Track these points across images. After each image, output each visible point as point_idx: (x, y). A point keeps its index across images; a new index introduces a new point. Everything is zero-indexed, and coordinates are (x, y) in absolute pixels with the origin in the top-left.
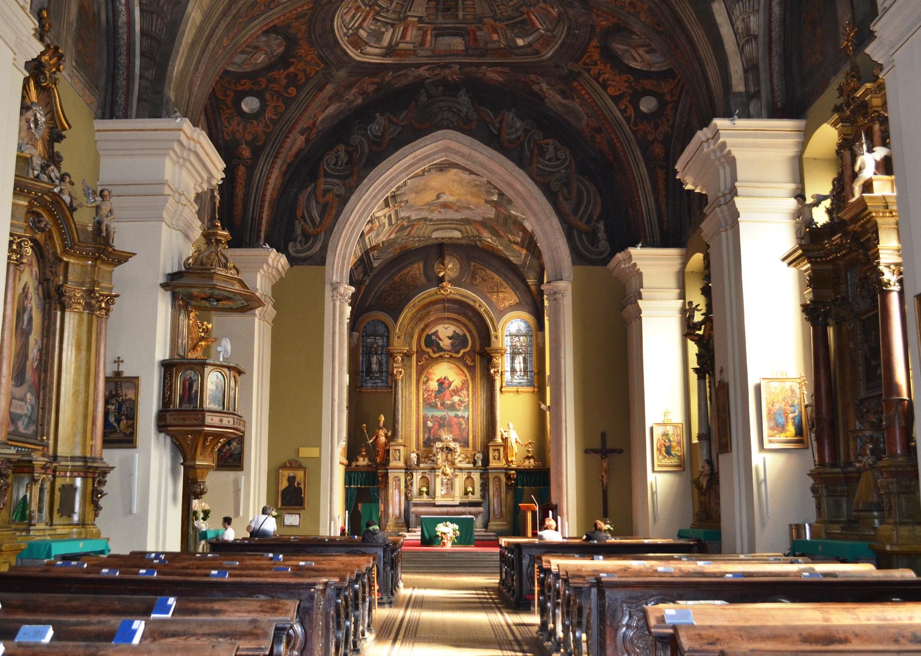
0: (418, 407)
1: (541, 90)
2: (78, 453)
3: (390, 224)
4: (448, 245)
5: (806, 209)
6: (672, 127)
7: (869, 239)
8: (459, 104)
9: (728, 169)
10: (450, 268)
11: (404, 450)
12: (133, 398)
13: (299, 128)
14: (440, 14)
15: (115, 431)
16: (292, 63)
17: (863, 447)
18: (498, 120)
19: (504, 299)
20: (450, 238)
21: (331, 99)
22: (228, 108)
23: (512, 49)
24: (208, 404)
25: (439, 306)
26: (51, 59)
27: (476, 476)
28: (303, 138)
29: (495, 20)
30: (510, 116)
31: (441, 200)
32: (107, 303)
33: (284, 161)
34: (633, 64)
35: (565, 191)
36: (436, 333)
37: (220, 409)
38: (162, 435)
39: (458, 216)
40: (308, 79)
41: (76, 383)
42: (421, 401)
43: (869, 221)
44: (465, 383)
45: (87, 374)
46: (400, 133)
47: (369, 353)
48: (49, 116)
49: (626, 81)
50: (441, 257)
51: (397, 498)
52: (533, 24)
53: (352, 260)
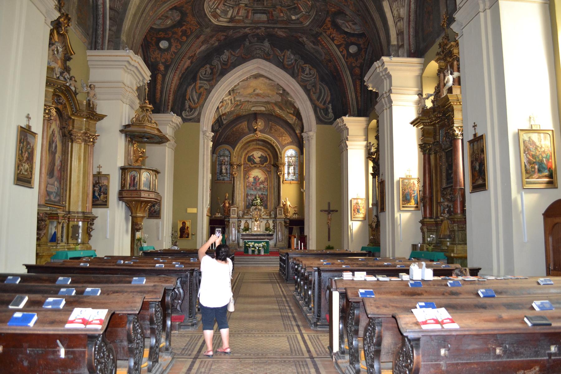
1: (303, 41)
2: (80, 210)
3: (231, 103)
9: (388, 80)
10: (260, 124)
13: (187, 56)
15: (98, 200)
16: (184, 25)
17: (444, 210)
18: (283, 54)
19: (285, 140)
20: (260, 111)
21: (203, 43)
23: (290, 21)
25: (255, 143)
27: (271, 222)
28: (189, 61)
32: (93, 139)
33: (180, 72)
34: (346, 30)
35: (314, 89)
36: (253, 155)
37: (148, 189)
38: (121, 202)
39: (264, 100)
40: (192, 33)
43: (450, 106)
44: (266, 179)
47: (221, 164)
52: (300, 9)
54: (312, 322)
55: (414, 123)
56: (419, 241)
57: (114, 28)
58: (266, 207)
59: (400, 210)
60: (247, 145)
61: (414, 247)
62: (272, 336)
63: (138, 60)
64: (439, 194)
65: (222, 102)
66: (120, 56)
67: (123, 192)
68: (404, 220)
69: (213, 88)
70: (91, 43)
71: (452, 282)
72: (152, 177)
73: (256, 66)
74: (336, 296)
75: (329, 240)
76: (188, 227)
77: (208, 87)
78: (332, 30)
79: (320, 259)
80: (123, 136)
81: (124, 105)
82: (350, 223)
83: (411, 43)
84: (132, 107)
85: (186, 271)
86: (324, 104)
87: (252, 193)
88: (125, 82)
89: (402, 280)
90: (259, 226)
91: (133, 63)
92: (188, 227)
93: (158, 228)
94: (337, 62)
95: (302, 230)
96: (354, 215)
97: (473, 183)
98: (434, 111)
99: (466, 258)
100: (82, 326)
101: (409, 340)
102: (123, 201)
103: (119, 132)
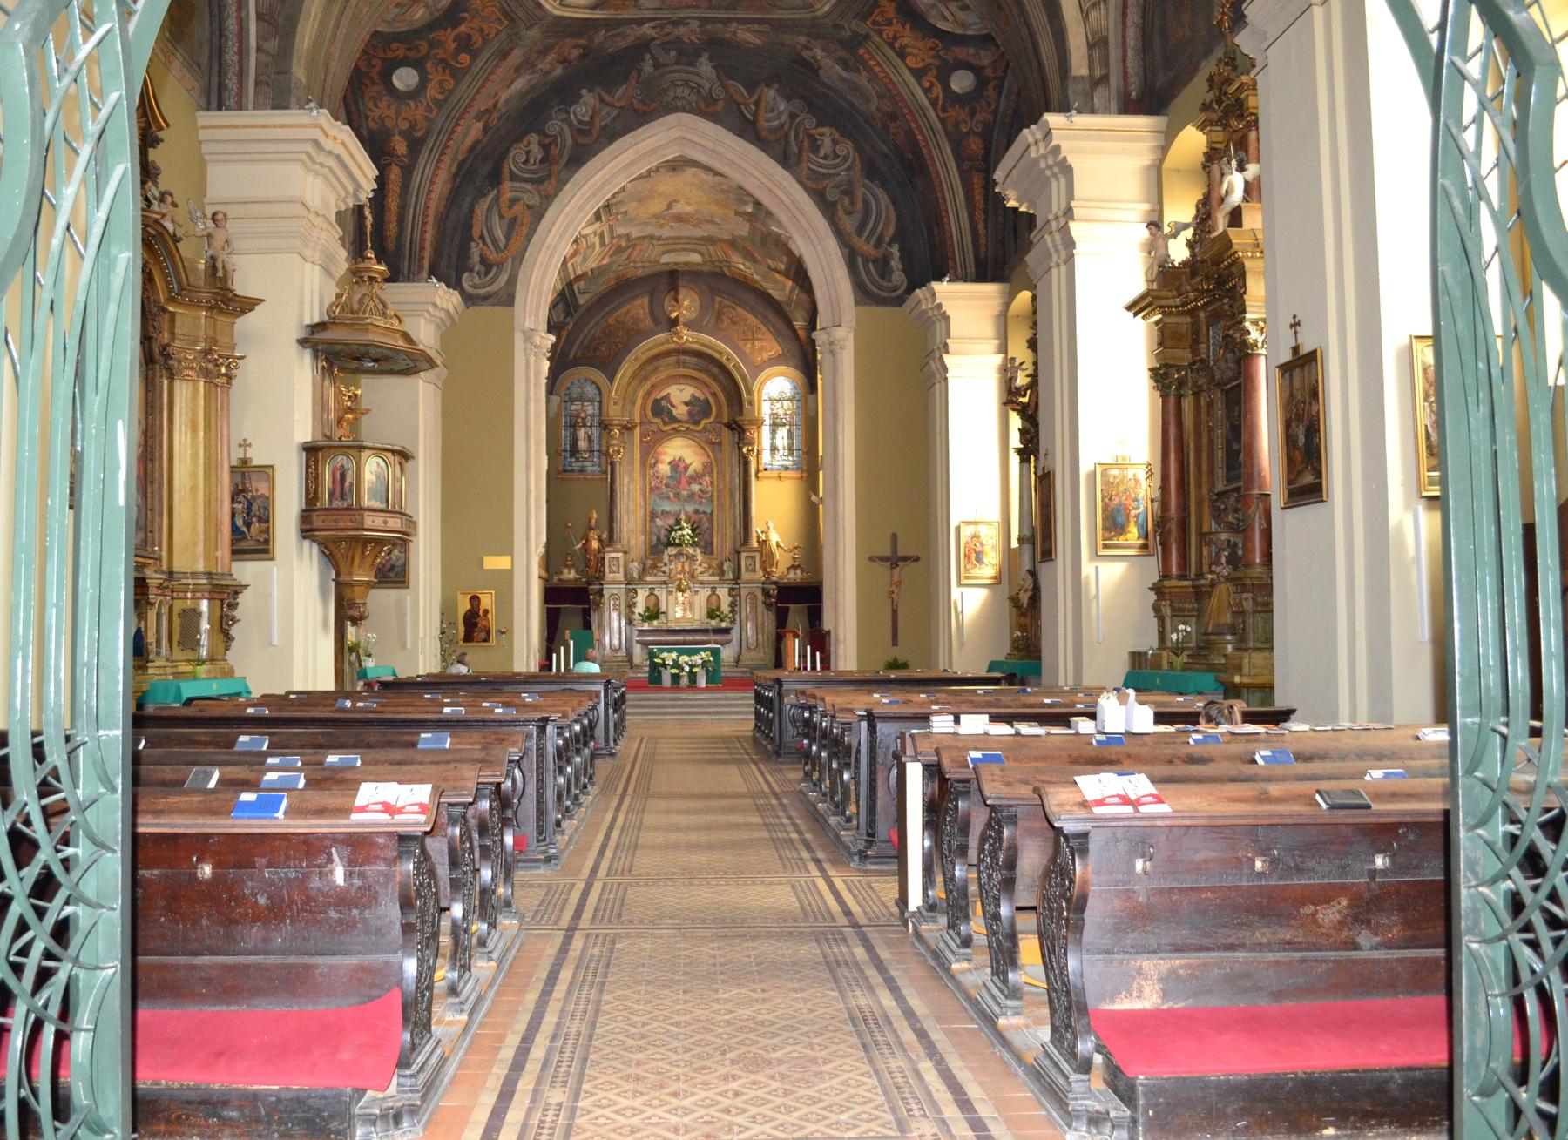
1: (814, 57)
2: (201, 568)
3: (603, 244)
4: (684, 273)
6: (995, 113)
7: (1234, 286)
8: (698, 75)
9: (1063, 181)
10: (687, 305)
13: (473, 112)
15: (245, 538)
17: (1218, 555)
18: (755, 97)
19: (762, 349)
20: (686, 264)
21: (518, 70)
22: (373, 83)
25: (672, 359)
27: (723, 593)
28: (480, 125)
32: (228, 367)
33: (455, 159)
34: (941, 25)
35: (846, 201)
36: (667, 397)
37: (383, 506)
38: (306, 543)
39: (698, 233)
40: (486, 42)
43: (1234, 263)
44: (707, 467)
46: (614, 119)
47: (574, 425)
53: (548, 297)
54: (854, 849)
55: (1136, 307)
56: (1149, 643)
58: (708, 549)
59: (1095, 555)
60: (652, 367)
61: (1137, 658)
62: (753, 883)
63: (342, 138)
64: (1206, 509)
65: (576, 241)
66: (291, 126)
67: (314, 515)
68: (1108, 583)
70: (207, 92)
71: (1200, 736)
72: (393, 471)
73: (675, 133)
74: (914, 772)
75: (895, 642)
76: (486, 611)
77: (536, 201)
78: (898, 27)
79: (870, 693)
80: (307, 354)
81: (308, 266)
82: (956, 592)
83: (1131, 72)
84: (327, 271)
85: (527, 723)
86: (877, 245)
87: (667, 508)
88: (308, 200)
89: (1077, 734)
90: (690, 606)
91: (328, 144)
92: (486, 611)
93: (401, 615)
94: (916, 121)
95: (815, 615)
96: (967, 570)
97: (1290, 482)
98: (1194, 274)
99: (1271, 688)
100: (386, 816)
101: (1066, 838)
102: (314, 540)
103: (295, 345)
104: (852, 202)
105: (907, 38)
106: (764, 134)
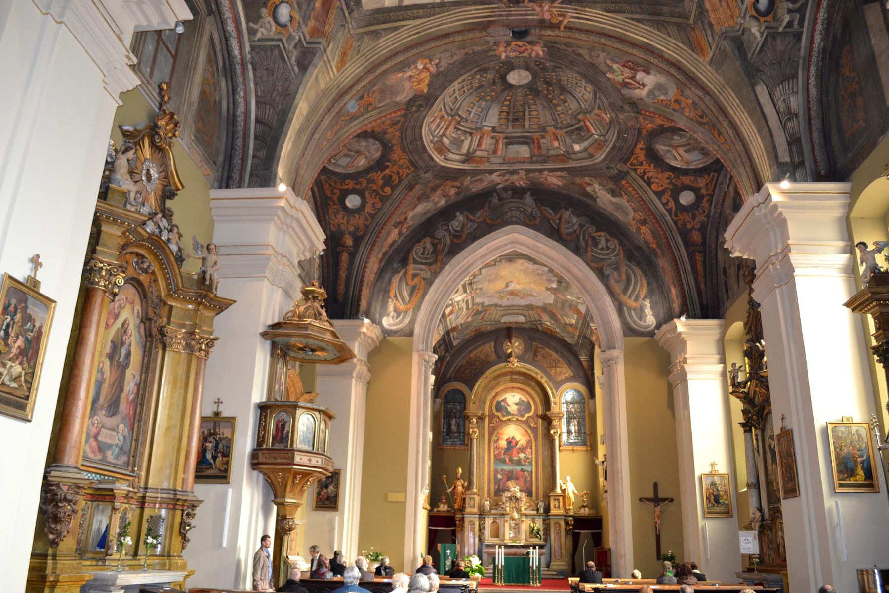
0: (489, 462)
1: (594, 191)
2: (166, 485)
3: (468, 308)
5: (869, 256)
6: (708, 216)
10: (515, 346)
11: (478, 498)
12: (230, 437)
13: (392, 222)
14: (510, 124)
16: (388, 167)
18: (558, 217)
19: (561, 372)
20: (516, 323)
22: (334, 204)
23: (569, 155)
24: (299, 444)
25: (508, 377)
26: (167, 124)
28: (396, 231)
29: (556, 128)
30: (567, 214)
31: (510, 288)
32: (207, 345)
34: (673, 163)
36: (504, 400)
37: (310, 449)
38: (256, 472)
39: (523, 302)
40: (400, 181)
41: (170, 417)
42: (492, 457)
45: (183, 411)
46: (476, 228)
48: (163, 174)
49: (667, 179)
50: (509, 338)
51: (472, 540)
52: (589, 131)
55: (847, 305)
57: (262, 154)
67: (260, 453)
69: (436, 277)
78: (647, 166)
83: (819, 159)
95: (598, 539)
104: (620, 276)
105: (652, 171)
106: (564, 236)
